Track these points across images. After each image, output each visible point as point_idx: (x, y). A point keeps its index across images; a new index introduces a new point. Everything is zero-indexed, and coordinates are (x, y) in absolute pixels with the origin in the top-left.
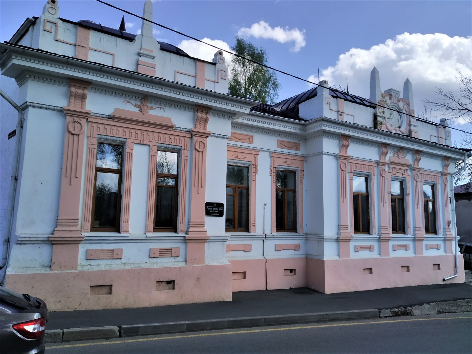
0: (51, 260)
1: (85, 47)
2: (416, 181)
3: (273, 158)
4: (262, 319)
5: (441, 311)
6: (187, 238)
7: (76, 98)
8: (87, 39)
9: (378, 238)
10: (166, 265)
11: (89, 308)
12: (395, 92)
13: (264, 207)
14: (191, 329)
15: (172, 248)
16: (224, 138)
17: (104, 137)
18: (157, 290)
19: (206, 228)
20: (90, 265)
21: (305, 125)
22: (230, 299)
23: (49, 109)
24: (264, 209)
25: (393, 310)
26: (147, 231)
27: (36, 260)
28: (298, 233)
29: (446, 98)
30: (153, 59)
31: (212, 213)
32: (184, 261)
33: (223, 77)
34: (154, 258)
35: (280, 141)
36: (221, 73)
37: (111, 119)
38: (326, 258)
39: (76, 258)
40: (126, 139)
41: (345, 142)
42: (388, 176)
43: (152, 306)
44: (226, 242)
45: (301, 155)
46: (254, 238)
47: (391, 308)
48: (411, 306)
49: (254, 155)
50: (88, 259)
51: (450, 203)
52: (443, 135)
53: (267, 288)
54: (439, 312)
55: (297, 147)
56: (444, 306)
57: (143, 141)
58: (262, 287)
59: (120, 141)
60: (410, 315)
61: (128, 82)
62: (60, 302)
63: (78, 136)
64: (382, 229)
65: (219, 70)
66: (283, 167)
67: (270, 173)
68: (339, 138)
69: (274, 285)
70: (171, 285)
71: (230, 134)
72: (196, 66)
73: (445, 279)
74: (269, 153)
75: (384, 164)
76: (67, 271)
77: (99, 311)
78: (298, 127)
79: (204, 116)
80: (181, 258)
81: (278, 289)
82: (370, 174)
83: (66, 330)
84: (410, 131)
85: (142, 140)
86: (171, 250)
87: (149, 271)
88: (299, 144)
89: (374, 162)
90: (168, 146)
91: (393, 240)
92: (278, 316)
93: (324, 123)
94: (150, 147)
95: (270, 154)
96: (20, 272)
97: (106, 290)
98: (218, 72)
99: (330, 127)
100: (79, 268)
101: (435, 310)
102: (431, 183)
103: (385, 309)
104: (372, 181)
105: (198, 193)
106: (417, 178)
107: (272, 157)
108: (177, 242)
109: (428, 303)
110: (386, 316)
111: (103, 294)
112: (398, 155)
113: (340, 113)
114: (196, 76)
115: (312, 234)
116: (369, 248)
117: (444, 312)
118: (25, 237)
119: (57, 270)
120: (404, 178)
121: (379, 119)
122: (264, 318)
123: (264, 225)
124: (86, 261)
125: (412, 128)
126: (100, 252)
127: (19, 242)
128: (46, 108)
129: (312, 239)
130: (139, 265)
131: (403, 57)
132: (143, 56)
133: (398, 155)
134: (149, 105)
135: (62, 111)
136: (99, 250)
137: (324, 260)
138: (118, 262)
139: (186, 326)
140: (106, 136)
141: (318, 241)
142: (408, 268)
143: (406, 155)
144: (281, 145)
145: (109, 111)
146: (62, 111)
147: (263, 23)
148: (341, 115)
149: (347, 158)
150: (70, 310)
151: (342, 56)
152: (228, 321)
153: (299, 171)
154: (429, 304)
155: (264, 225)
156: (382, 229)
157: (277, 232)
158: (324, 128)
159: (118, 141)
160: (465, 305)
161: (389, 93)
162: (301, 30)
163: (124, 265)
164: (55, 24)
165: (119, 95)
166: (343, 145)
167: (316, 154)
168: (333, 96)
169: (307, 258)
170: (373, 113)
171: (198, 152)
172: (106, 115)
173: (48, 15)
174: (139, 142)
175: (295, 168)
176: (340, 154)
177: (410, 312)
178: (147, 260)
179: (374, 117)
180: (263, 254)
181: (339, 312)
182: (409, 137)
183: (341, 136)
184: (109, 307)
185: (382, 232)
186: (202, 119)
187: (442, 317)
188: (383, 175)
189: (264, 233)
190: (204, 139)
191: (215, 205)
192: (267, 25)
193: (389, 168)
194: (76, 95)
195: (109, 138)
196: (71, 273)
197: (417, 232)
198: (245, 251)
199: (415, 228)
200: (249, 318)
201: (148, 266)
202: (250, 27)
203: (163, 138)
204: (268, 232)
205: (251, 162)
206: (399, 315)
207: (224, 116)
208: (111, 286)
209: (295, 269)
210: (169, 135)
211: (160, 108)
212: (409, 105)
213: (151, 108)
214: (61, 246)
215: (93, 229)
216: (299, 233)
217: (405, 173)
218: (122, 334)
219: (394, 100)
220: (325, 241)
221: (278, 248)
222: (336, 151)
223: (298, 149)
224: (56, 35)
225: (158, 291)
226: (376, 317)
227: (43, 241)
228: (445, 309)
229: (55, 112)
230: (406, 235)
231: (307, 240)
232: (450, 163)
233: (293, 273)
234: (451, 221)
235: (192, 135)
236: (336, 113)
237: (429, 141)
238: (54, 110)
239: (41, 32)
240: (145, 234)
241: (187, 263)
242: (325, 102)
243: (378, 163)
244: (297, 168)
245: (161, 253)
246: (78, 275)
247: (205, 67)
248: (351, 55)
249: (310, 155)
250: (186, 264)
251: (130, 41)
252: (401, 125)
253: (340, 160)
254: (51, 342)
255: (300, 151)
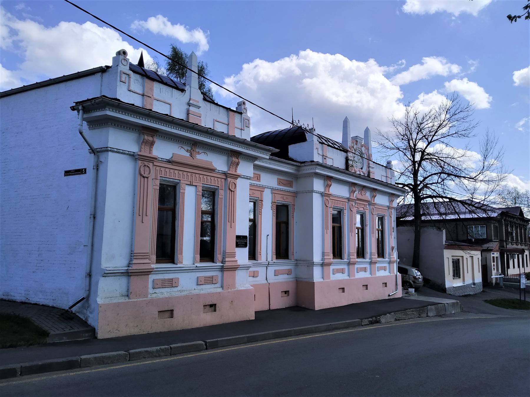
0: (128, 290)
1: (151, 97)
2: (351, 211)
3: (274, 194)
4: (292, 330)
5: (397, 319)
6: (224, 267)
7: (146, 144)
8: (152, 89)
9: (348, 262)
10: (209, 291)
11: (158, 331)
12: (360, 138)
13: (267, 238)
14: (250, 340)
15: (213, 276)
16: (247, 179)
17: (164, 178)
18: (204, 313)
19: (237, 258)
20: (156, 293)
21: (299, 166)
22: (253, 318)
23: (124, 154)
24: (267, 239)
25: (370, 319)
26: (196, 261)
27: (117, 291)
28: (290, 259)
29: (383, 138)
30: (199, 108)
31: (239, 244)
32: (221, 286)
33: (247, 125)
34: (200, 285)
35: (279, 179)
36: (246, 121)
37: (170, 162)
38: (315, 281)
39: (147, 287)
40: (180, 180)
41: (235, 159)
42: (355, 210)
43: (201, 327)
44: (249, 269)
45: (293, 191)
46: (260, 265)
47: (368, 318)
48: (379, 316)
49: (260, 192)
50: (155, 288)
51: (393, 232)
52: (389, 176)
53: (270, 308)
54: (396, 320)
55: (290, 184)
56: (400, 315)
57: (192, 182)
58: (266, 308)
59: (175, 182)
60: (379, 323)
61: (137, 117)
62: (137, 326)
63: (147, 178)
64: (351, 255)
65: (245, 119)
66: (281, 202)
67: (271, 208)
68: (228, 154)
69: (275, 306)
70: (213, 308)
71: (252, 175)
72: (228, 115)
73: (390, 295)
74: (271, 190)
75: (353, 200)
76: (141, 299)
77: (165, 332)
78: (294, 167)
79: (150, 139)
80: (218, 285)
81: (277, 308)
82: (343, 208)
83: (172, 346)
84: (369, 173)
85: (192, 181)
86: (212, 278)
87: (198, 296)
88: (292, 182)
89: (221, 173)
90: (209, 186)
91: (155, 273)
92: (301, 328)
93: (318, 167)
94: (196, 187)
95: (271, 191)
96: (107, 301)
97: (168, 314)
98: (244, 120)
99: (241, 148)
100: (149, 296)
101: (394, 318)
102: (337, 209)
103: (365, 319)
104: (344, 214)
105: (143, 223)
106: (327, 204)
107: (273, 193)
108: (216, 271)
109: (389, 313)
110: (366, 324)
111: (166, 318)
112: (361, 192)
113: (324, 157)
114: (229, 124)
115: (302, 260)
116: (170, 284)
117: (399, 320)
118: (110, 270)
119: (134, 299)
120: (364, 212)
121: (350, 163)
122: (294, 330)
123: (267, 253)
124: (152, 289)
125: (371, 170)
126: (164, 281)
127: (105, 275)
128: (122, 153)
129: (302, 265)
130: (191, 291)
131: (307, 74)
132: (192, 106)
133: (361, 192)
134: (197, 150)
135: (132, 155)
136: (162, 280)
137: (314, 281)
138: (175, 289)
139: (247, 338)
140: (165, 178)
141: (308, 266)
142: (366, 287)
143: (367, 192)
144: (280, 183)
145: (168, 157)
146: (132, 155)
147: (160, 17)
148: (325, 159)
149: (329, 195)
150: (144, 333)
151: (245, 66)
152: (272, 333)
153: (292, 205)
154: (390, 314)
155: (267, 253)
156: (351, 255)
157: (276, 259)
158: (317, 171)
159: (173, 182)
160: (411, 314)
161: (356, 139)
162: (205, 32)
163: (180, 292)
164: (129, 75)
165: (130, 129)
166: (328, 184)
167: (307, 192)
168: (320, 143)
169: (297, 281)
170: (345, 157)
171: (144, 178)
172: (166, 159)
173: (122, 67)
174: (189, 183)
175: (289, 203)
176: (140, 153)
177: (379, 321)
178: (195, 287)
179: (346, 160)
180: (267, 279)
181: (338, 323)
182: (368, 177)
183: (326, 177)
184: (171, 329)
185: (391, 257)
186: (235, 163)
187: (398, 323)
188: (352, 210)
189: (267, 261)
190: (235, 180)
191: (242, 237)
192: (165, 20)
193: (355, 203)
194: (147, 142)
195: (168, 179)
196: (145, 300)
197: (326, 257)
198: (253, 277)
199: (371, 253)
200: (284, 330)
201: (196, 292)
202: (146, 20)
203: (178, 173)
204: (269, 259)
205: (259, 198)
206: (373, 323)
207: (224, 153)
208: (172, 311)
209: (289, 291)
210: (183, 172)
211: (204, 153)
212: (368, 150)
213: (199, 153)
214: (136, 277)
215: (158, 262)
216: (344, 260)
217: (365, 207)
218: (208, 347)
219: (359, 145)
220: (315, 266)
221: (276, 273)
222: (322, 189)
223: (291, 186)
224: (129, 86)
225: (205, 314)
226: (360, 325)
227: (122, 273)
228: (399, 317)
229: (127, 156)
230: (364, 259)
231: (296, 265)
232: (377, 195)
233: (287, 295)
234: (394, 247)
235: (226, 176)
236: (322, 156)
237: (379, 180)
238: (127, 154)
239: (119, 83)
240: (194, 264)
241: (372, 275)
242: (315, 148)
243: (349, 199)
244: (290, 203)
245: (206, 280)
246: (150, 302)
247: (235, 116)
248: (256, 66)
249: (301, 192)
250: (223, 290)
251: (182, 92)
252: (363, 166)
253: (325, 197)
254: (164, 356)
255: (292, 188)
